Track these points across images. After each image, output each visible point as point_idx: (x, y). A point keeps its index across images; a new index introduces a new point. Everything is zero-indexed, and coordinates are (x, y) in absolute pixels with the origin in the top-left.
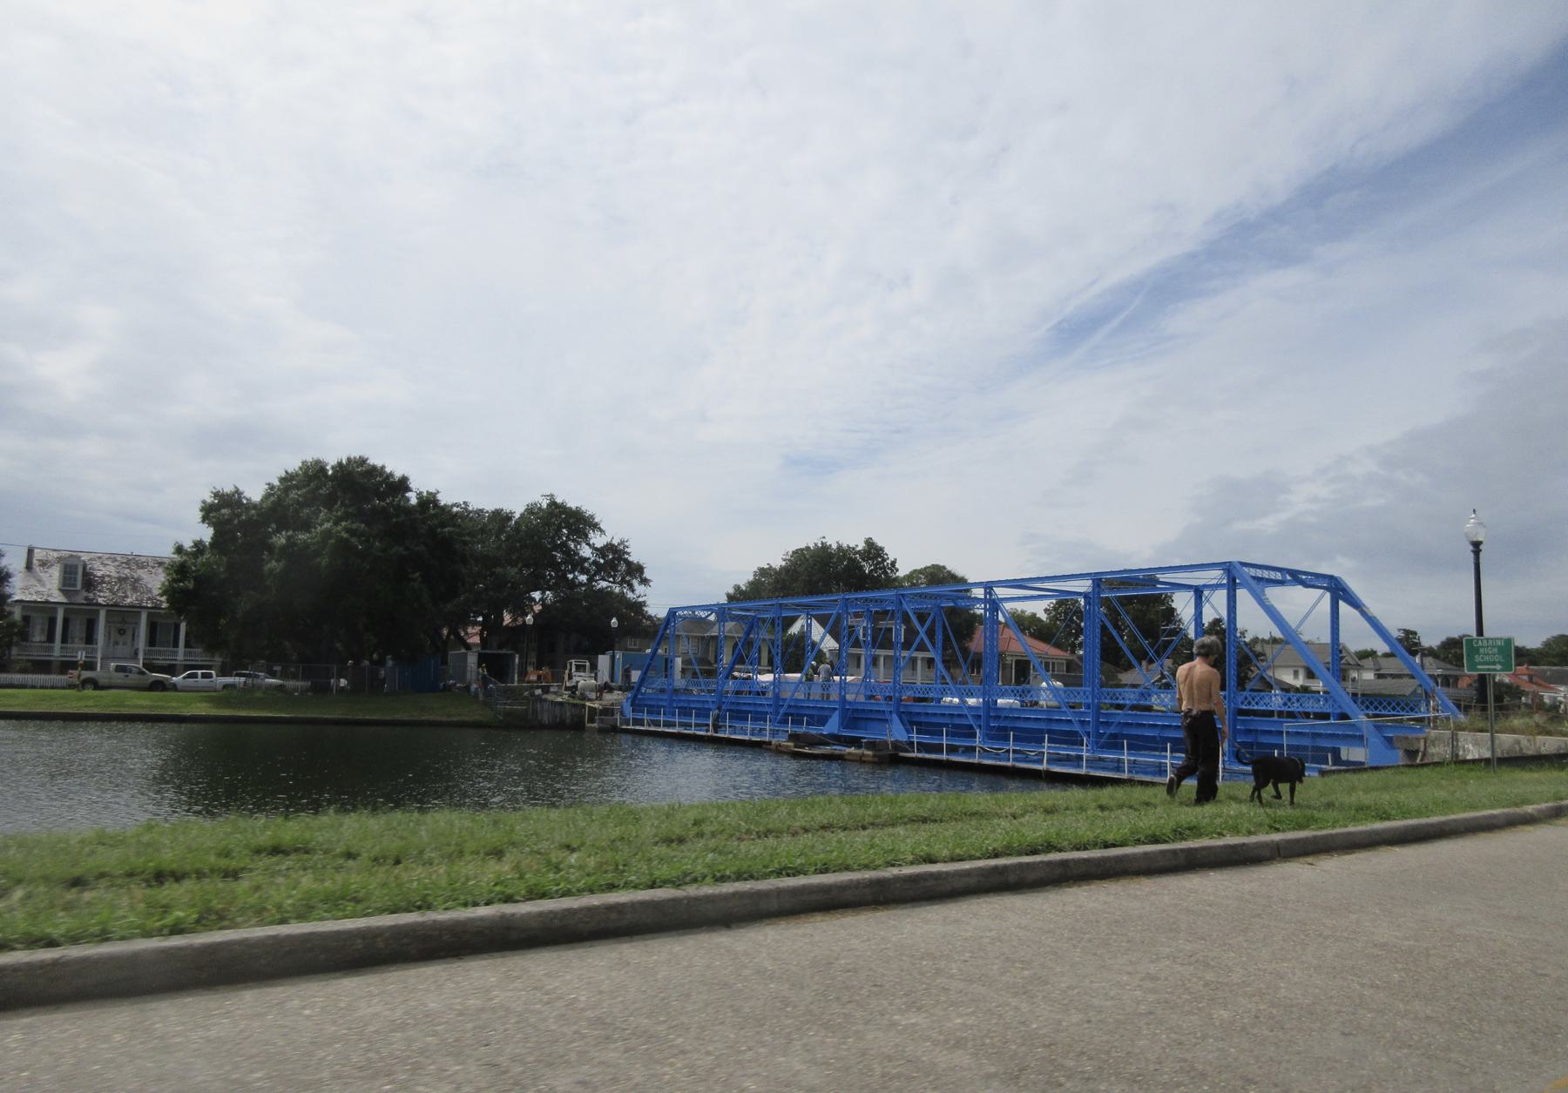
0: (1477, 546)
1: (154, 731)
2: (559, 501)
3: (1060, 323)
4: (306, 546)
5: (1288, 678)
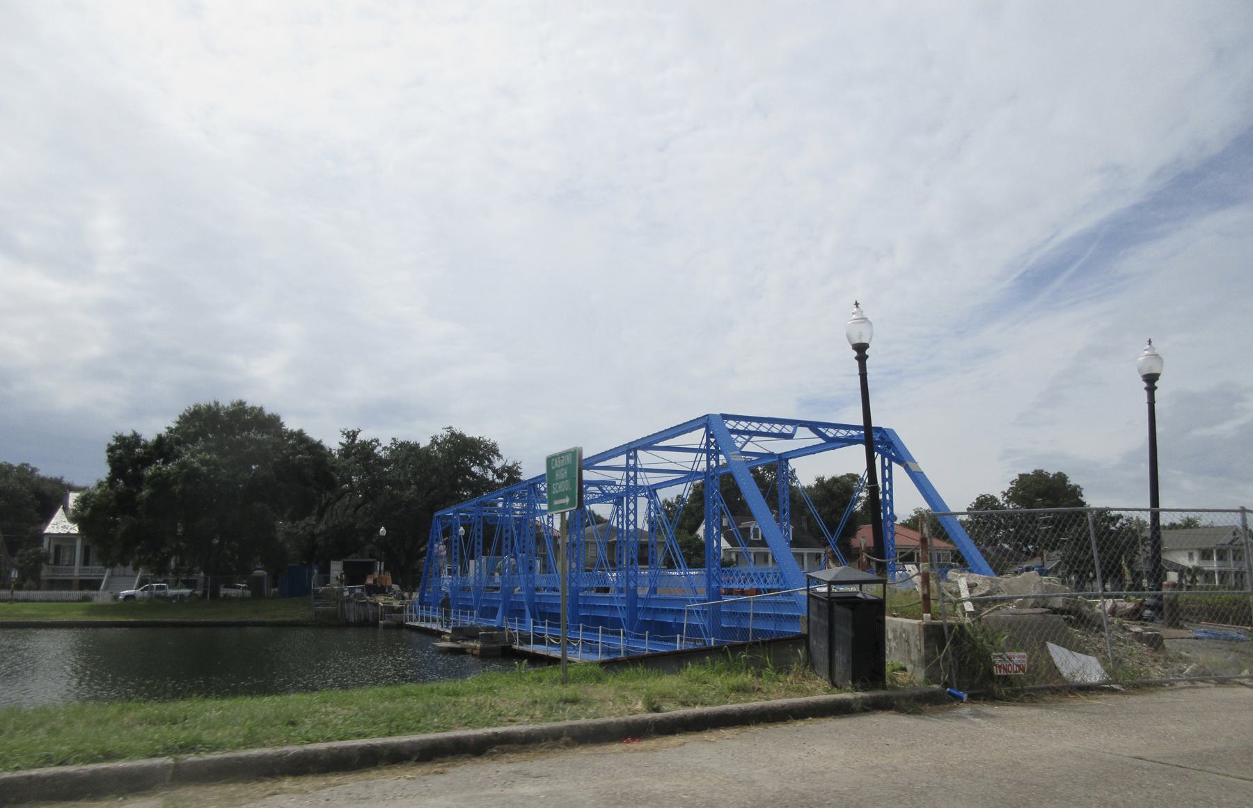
0: (861, 350)
1: (63, 633)
2: (457, 432)
3: (1025, 273)
4: (169, 474)
5: (1184, 560)
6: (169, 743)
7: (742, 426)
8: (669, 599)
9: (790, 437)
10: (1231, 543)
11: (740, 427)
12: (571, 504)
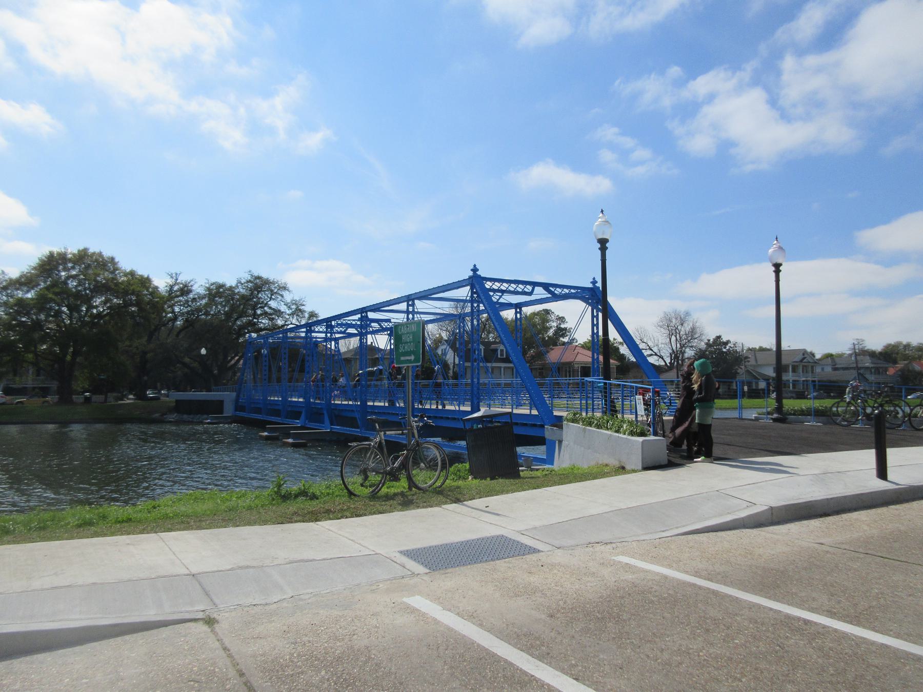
6: (87, 508)
7: (496, 286)
8: (730, 529)
9: (530, 294)
10: (801, 361)
11: (495, 287)
12: (416, 360)
